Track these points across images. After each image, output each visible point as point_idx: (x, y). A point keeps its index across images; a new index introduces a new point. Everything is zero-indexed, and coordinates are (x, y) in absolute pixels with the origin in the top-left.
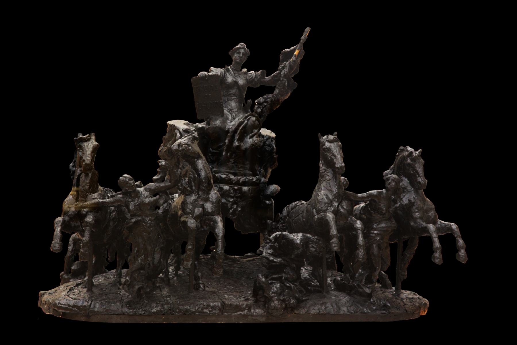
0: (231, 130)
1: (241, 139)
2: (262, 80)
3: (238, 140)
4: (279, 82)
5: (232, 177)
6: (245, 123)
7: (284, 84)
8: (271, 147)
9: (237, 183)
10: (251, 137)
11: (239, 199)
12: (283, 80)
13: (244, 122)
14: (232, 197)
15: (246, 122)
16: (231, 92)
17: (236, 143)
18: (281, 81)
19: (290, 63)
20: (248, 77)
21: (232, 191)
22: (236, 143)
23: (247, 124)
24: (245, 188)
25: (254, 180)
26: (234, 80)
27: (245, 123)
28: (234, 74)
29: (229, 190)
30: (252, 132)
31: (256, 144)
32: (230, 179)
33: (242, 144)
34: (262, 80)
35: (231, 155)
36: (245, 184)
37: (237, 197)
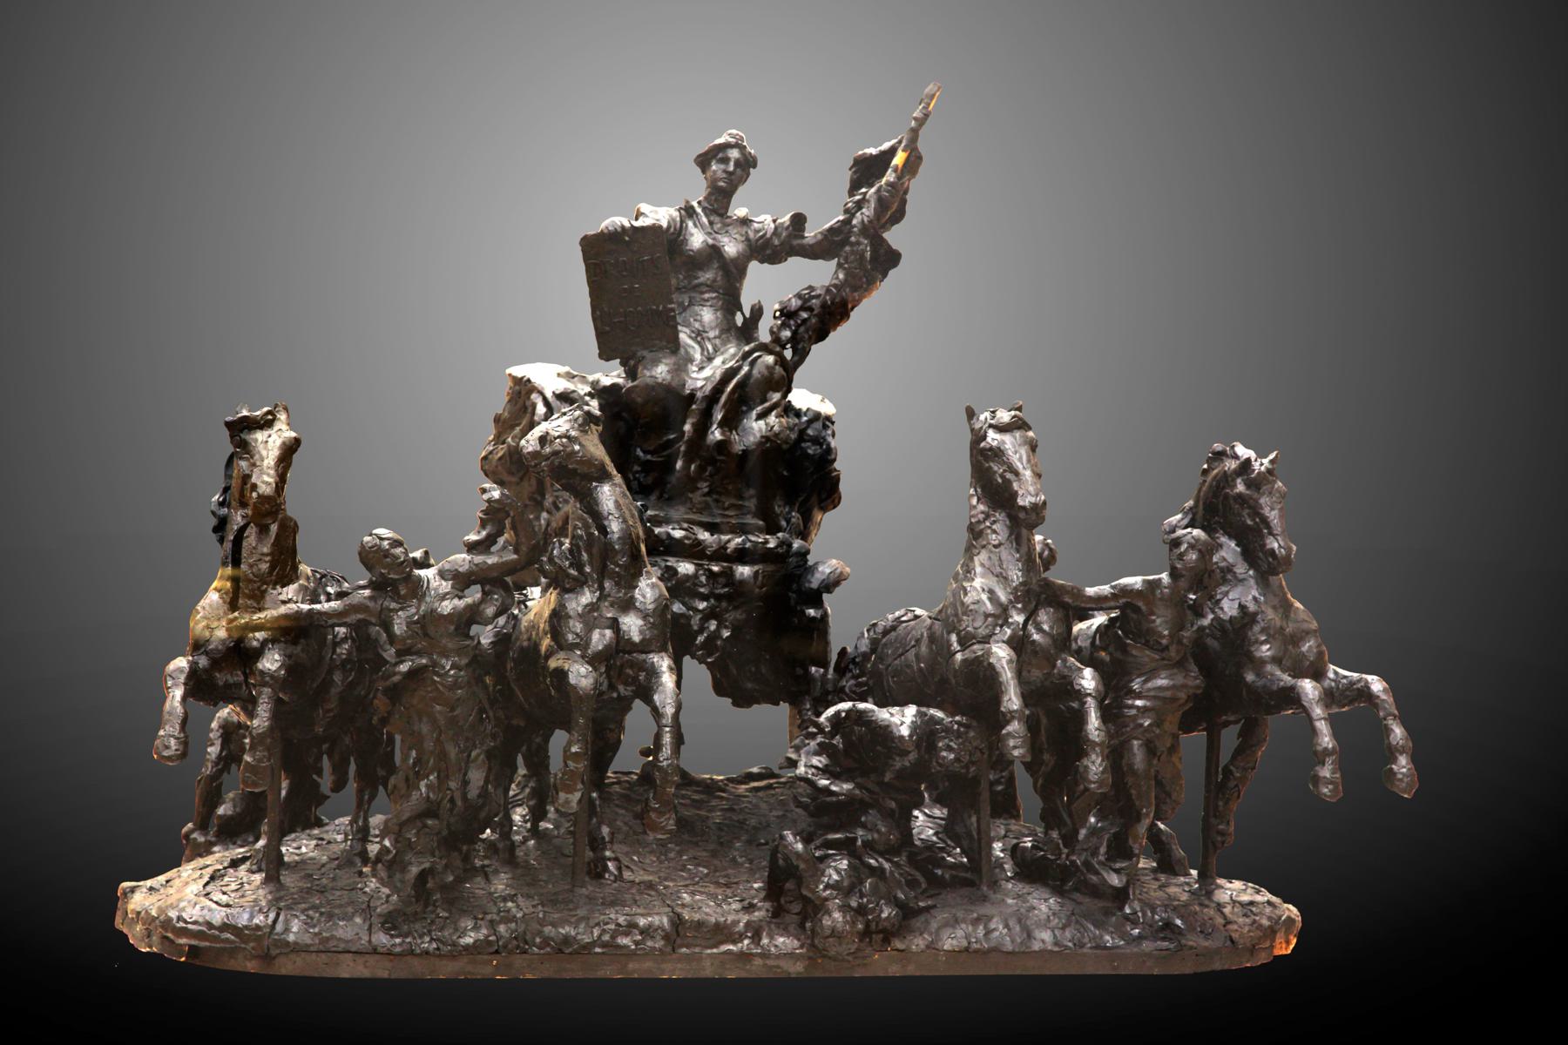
0: (699, 394)
1: (732, 421)
2: (795, 242)
3: (721, 425)
4: (848, 248)
5: (704, 536)
6: (743, 372)
7: (862, 256)
8: (821, 445)
9: (720, 554)
10: (761, 416)
11: (724, 604)
12: (858, 243)
13: (740, 368)
14: (704, 598)
15: (746, 368)
16: (702, 280)
17: (716, 434)
18: (852, 244)
19: (879, 190)
20: (751, 235)
21: (703, 579)
22: (716, 434)
23: (748, 375)
24: (744, 571)
25: (771, 545)
26: (710, 241)
27: (743, 372)
28: (711, 223)
29: (696, 576)
30: (764, 400)
31: (776, 435)
32: (699, 543)
33: (735, 437)
34: (795, 242)
35: (701, 469)
36: (742, 556)
37: (719, 598)
